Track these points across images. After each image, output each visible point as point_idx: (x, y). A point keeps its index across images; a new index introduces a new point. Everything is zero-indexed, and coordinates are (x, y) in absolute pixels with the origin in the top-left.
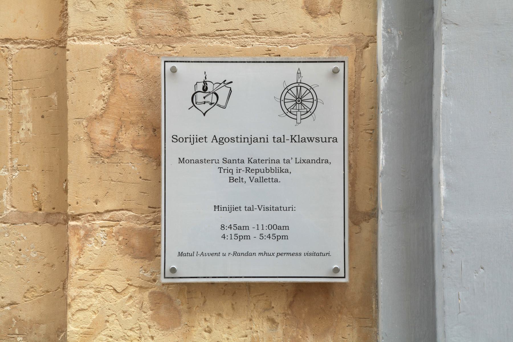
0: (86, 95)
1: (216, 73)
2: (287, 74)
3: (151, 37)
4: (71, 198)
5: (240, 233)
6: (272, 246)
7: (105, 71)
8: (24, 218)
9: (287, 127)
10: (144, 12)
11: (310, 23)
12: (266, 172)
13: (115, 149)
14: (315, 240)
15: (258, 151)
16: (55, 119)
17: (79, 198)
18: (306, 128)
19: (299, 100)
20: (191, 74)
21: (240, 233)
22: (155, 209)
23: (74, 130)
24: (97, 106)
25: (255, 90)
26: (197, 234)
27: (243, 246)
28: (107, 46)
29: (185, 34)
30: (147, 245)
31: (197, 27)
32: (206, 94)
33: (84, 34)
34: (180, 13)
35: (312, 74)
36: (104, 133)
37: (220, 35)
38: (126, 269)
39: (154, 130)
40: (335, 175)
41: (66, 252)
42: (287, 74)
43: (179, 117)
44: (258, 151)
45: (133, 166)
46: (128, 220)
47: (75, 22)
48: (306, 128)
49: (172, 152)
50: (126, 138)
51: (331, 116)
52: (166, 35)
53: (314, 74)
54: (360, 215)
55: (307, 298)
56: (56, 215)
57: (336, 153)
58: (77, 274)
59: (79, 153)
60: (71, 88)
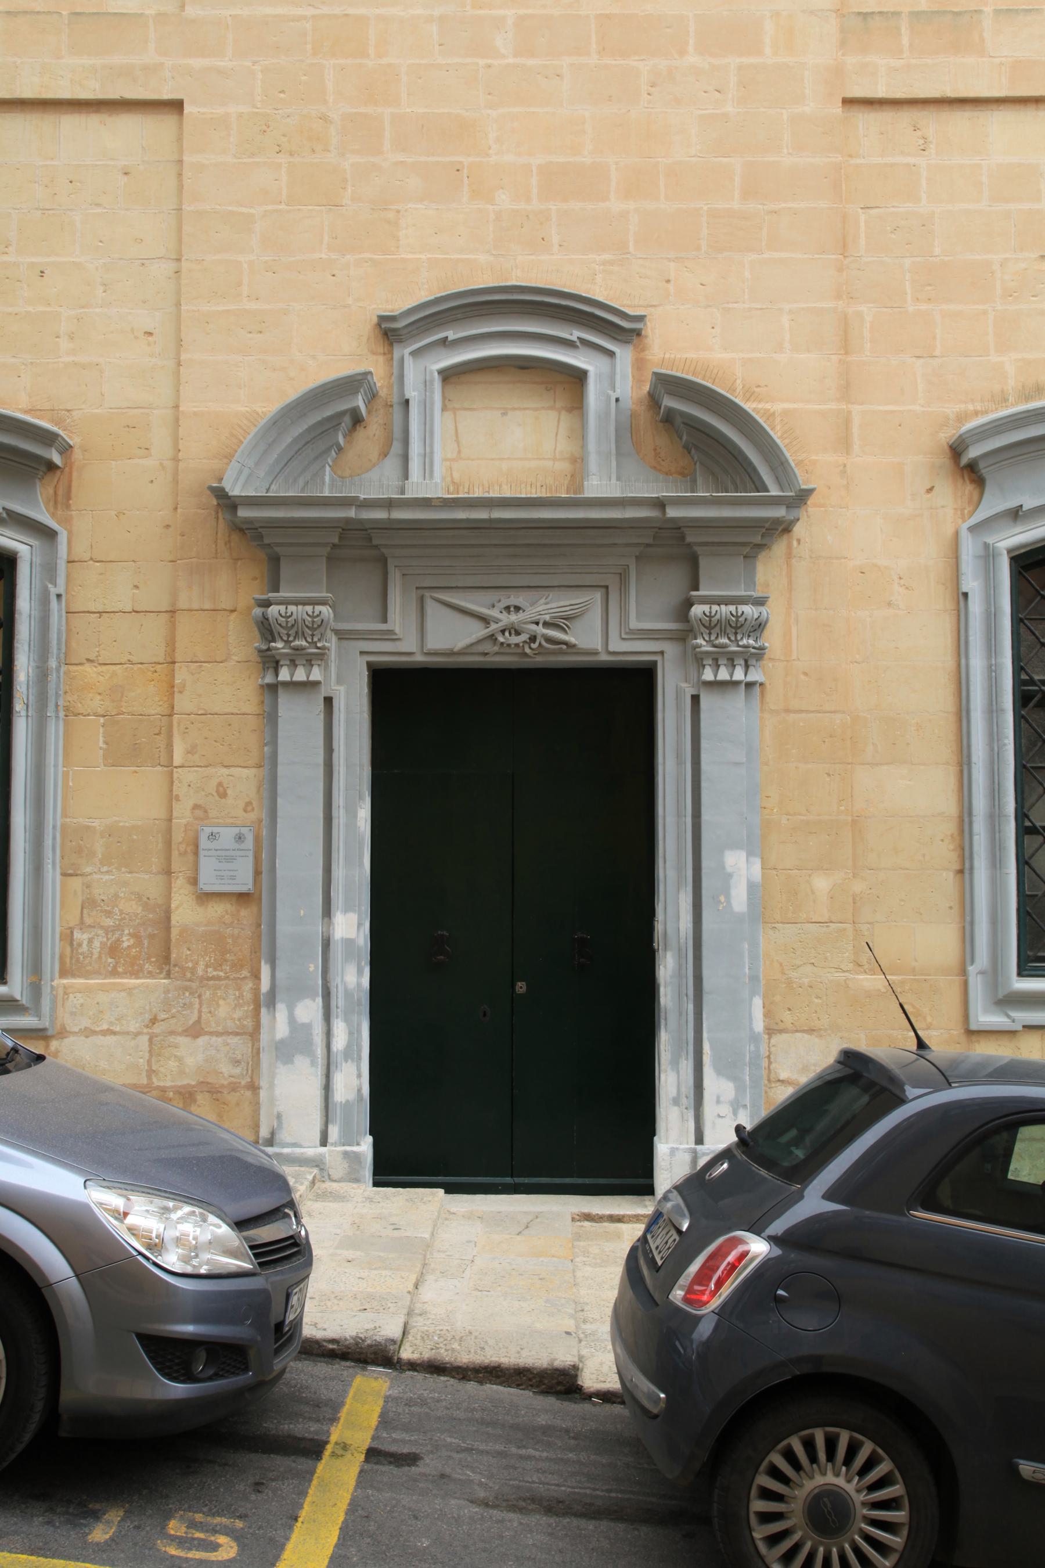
0: (178, 836)
1: (215, 830)
2: (236, 830)
3: (197, 819)
4: (173, 866)
5: (221, 877)
6: (230, 881)
7: (183, 829)
8: (159, 873)
9: (236, 846)
10: (675, 1193)
11: (245, 815)
12: (230, 859)
13: (186, 852)
14: (244, 882)
15: (227, 853)
16: (168, 843)
17: (175, 867)
18: (243, 846)
19: (240, 838)
20: (208, 830)
21: (221, 877)
22: (196, 870)
23: (174, 846)
24: (181, 840)
25: (227, 835)
26: (208, 882)
27: (223, 882)
28: (184, 821)
29: (207, 818)
30: (194, 881)
31: (211, 815)
32: (212, 836)
33: (178, 818)
34: (206, 811)
35: (244, 830)
36: (182, 847)
37: (218, 818)
38: (188, 889)
39: (197, 846)
40: (251, 858)
41: (170, 884)
42: (236, 830)
43: (204, 843)
44: (227, 853)
45: (190, 857)
46: (189, 874)
47: (175, 814)
48: (243, 846)
49: (202, 853)
50: (189, 849)
51: (249, 843)
52: (130, 662)
53: (244, 830)
54: (257, 873)
55: (242, 898)
56: (168, 872)
57: (251, 854)
58: (174, 890)
59: (175, 853)
60: (173, 834)
